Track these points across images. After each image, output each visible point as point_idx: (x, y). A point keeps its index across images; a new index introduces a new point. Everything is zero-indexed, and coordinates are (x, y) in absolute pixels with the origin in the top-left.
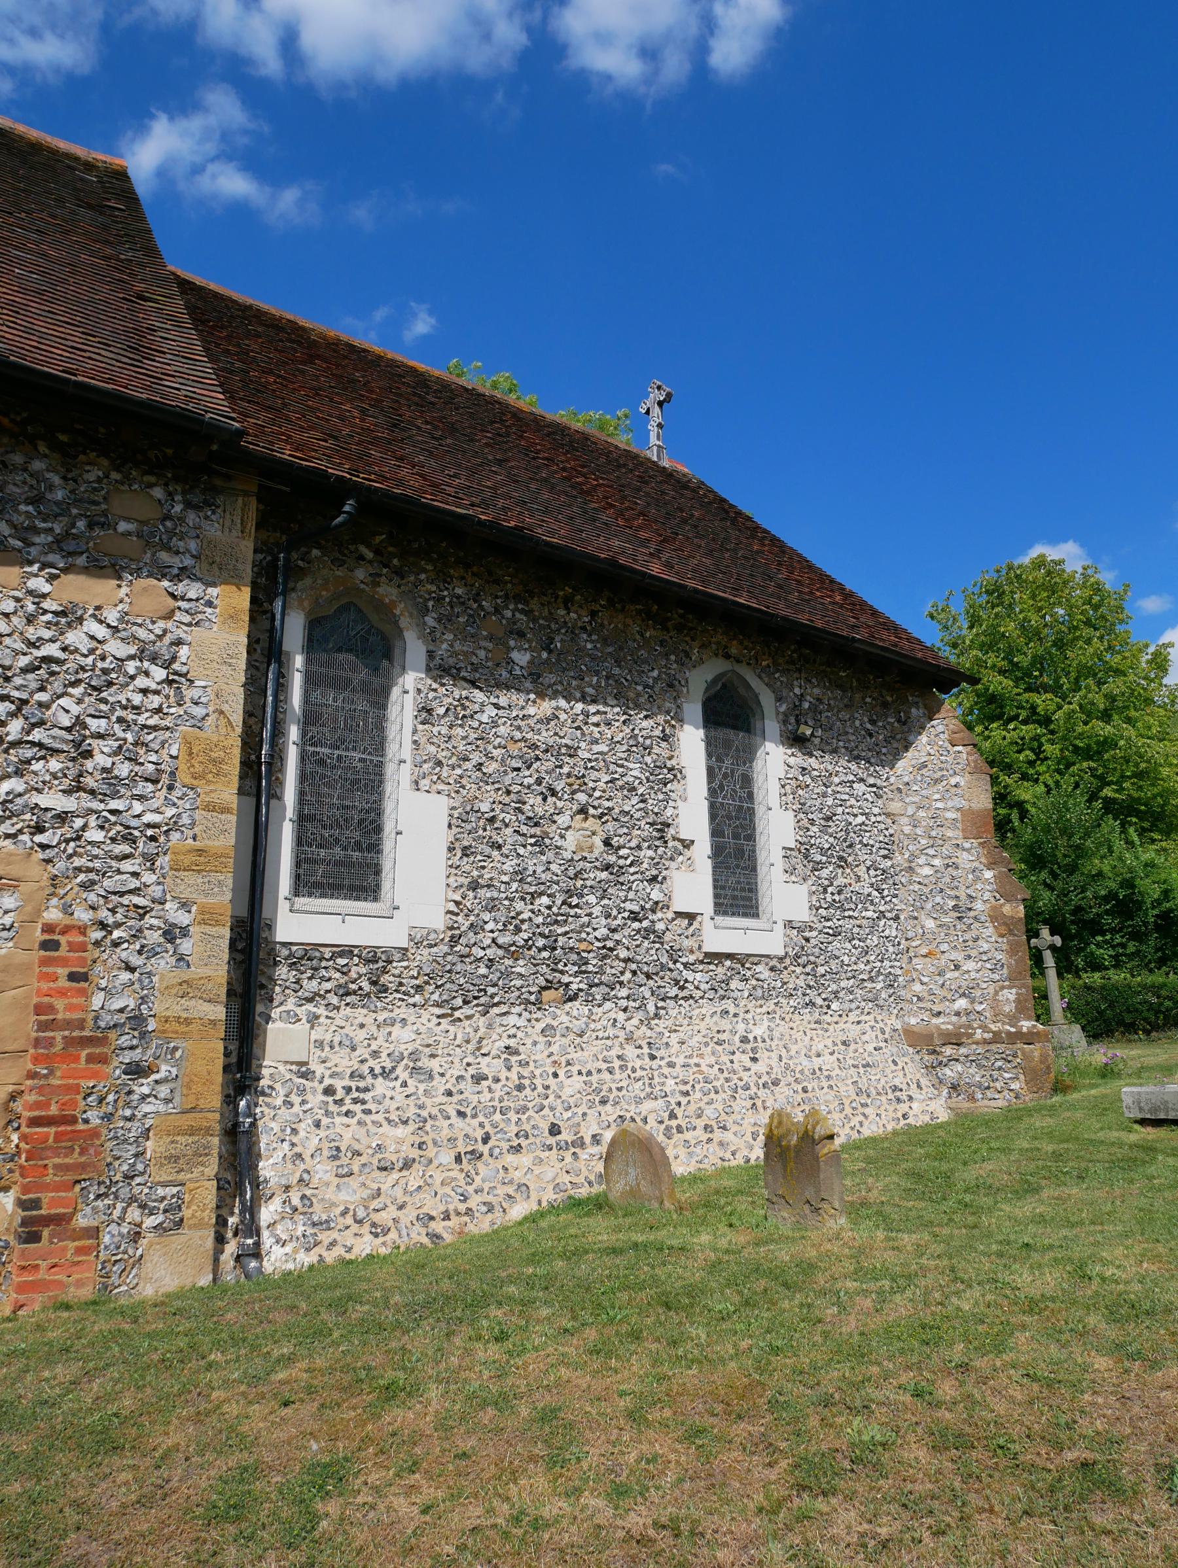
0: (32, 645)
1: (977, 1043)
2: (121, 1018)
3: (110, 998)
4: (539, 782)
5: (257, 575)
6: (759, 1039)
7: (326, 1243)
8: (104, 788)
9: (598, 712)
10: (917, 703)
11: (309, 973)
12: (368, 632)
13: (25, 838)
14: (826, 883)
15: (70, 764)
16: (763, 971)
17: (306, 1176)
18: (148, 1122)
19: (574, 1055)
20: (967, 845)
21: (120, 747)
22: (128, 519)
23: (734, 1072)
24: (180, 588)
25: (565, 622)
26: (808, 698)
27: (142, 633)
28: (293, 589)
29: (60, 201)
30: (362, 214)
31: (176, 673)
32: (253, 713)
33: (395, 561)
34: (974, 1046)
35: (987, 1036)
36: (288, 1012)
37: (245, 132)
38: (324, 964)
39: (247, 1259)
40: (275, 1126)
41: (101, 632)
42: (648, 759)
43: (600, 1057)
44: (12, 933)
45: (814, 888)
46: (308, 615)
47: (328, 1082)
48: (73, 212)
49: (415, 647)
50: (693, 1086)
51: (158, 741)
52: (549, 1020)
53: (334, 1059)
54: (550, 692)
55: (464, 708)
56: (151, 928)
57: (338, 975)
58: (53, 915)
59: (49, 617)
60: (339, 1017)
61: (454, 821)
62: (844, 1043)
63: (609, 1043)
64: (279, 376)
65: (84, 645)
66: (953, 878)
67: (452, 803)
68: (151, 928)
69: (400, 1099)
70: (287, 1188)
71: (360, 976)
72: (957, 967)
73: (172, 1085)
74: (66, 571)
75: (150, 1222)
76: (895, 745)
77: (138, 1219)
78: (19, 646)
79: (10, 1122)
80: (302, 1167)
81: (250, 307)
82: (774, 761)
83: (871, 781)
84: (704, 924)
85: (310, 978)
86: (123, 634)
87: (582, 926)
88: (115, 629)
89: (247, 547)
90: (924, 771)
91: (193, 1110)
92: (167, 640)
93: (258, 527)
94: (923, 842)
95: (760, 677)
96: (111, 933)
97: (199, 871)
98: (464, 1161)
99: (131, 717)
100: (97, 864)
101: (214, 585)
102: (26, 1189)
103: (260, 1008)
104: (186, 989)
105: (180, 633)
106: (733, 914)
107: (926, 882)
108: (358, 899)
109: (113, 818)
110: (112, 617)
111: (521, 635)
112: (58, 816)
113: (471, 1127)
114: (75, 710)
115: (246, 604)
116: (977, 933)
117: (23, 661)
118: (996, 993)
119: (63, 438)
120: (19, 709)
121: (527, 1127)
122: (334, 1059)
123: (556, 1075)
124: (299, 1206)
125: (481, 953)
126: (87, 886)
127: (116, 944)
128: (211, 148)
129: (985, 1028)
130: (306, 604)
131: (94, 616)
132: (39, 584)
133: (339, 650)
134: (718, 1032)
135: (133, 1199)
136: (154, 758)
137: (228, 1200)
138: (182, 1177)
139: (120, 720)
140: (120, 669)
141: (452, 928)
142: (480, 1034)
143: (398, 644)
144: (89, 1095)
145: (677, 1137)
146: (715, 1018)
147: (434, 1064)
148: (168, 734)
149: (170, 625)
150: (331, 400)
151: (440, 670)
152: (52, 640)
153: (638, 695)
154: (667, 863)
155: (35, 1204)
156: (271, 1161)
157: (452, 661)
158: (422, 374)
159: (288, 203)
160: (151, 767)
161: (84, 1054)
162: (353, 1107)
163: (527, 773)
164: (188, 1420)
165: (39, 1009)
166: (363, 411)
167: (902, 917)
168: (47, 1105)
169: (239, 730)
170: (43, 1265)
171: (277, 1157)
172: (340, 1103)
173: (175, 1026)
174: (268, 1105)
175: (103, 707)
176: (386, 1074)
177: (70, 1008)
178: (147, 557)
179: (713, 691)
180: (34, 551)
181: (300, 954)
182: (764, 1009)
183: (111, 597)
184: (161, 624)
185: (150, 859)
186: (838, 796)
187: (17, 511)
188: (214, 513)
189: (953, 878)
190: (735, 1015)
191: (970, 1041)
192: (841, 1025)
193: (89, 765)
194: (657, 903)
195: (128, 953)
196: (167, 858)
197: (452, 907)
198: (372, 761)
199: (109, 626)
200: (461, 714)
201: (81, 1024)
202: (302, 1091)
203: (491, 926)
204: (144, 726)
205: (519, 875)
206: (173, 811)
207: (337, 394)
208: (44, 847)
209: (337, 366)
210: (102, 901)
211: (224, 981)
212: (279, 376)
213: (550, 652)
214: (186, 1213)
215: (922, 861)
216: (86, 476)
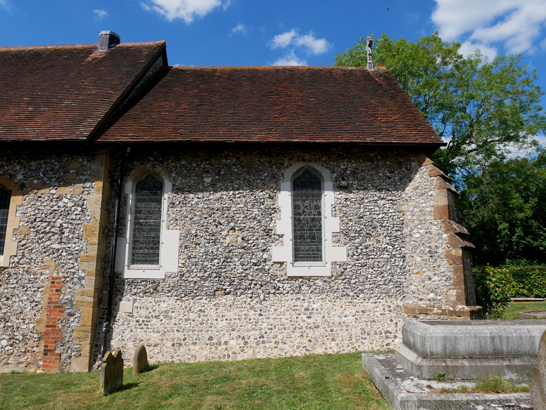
1: (435, 314)
2: (67, 301)
4: (214, 221)
6: (315, 309)
8: (67, 242)
9: (239, 193)
10: (414, 160)
14: (358, 245)
16: (319, 283)
17: (124, 346)
19: (226, 313)
20: (435, 223)
22: (73, 169)
23: (297, 322)
25: (226, 164)
26: (349, 169)
33: (160, 159)
34: (434, 316)
35: (440, 311)
40: (118, 330)
42: (262, 207)
43: (237, 314)
45: (350, 248)
49: (168, 185)
50: (275, 326)
52: (217, 301)
54: (219, 189)
55: (186, 201)
58: (55, 275)
60: (143, 300)
61: (182, 238)
62: (363, 312)
63: (242, 309)
66: (429, 238)
67: (181, 232)
69: (159, 325)
72: (430, 279)
76: (405, 180)
80: (124, 343)
82: (329, 198)
83: (390, 198)
84: (288, 265)
87: (232, 269)
90: (417, 191)
94: (417, 222)
95: (322, 165)
98: (175, 346)
101: (94, 182)
104: (83, 294)
106: (308, 260)
107: (417, 240)
108: (152, 264)
111: (208, 172)
113: (180, 335)
116: (439, 263)
118: (447, 291)
121: (200, 337)
123: (217, 320)
125: (191, 279)
129: (439, 308)
132: (53, 191)
134: (294, 306)
138: (81, 343)
140: (71, 210)
141: (180, 272)
142: (191, 305)
145: (262, 345)
146: (293, 301)
151: (177, 190)
153: (258, 184)
154: (270, 244)
157: (181, 186)
162: (144, 327)
163: (210, 218)
167: (407, 256)
169: (99, 222)
171: (117, 339)
173: (80, 303)
176: (156, 317)
177: (55, 298)
179: (296, 176)
180: (52, 183)
181: (131, 281)
182: (320, 297)
183: (67, 191)
186: (367, 207)
189: (429, 238)
190: (303, 300)
191: (431, 313)
192: (365, 304)
193: (64, 236)
194: (266, 259)
197: (181, 265)
200: (184, 203)
201: (57, 303)
203: (195, 270)
205: (206, 253)
213: (220, 175)
214: (82, 353)
215: (415, 231)
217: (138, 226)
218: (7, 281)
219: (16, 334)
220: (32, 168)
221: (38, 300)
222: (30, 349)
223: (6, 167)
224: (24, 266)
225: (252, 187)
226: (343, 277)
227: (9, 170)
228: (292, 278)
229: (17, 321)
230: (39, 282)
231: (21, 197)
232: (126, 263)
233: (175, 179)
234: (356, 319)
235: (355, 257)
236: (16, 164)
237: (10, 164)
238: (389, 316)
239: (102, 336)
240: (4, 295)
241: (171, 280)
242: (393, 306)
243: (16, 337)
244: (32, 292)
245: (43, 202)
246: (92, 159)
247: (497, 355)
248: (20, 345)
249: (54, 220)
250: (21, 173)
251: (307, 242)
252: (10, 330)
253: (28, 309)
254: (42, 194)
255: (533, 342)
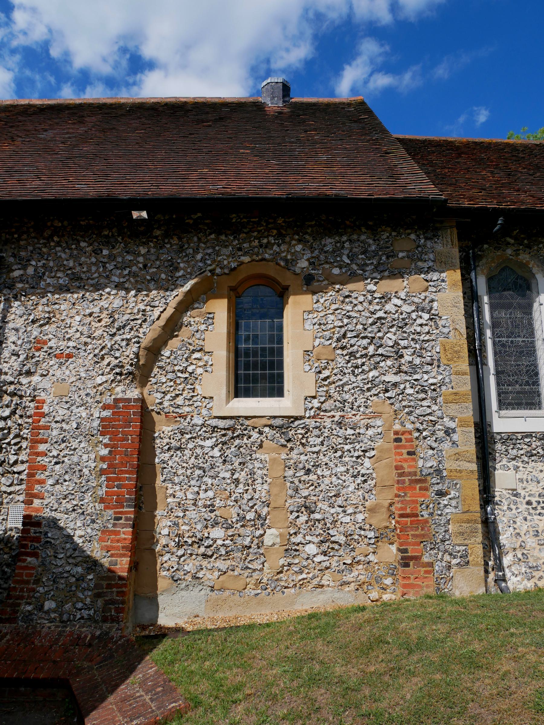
0: (372, 313)
2: (431, 471)
3: (426, 462)
5: (461, 262)
7: (537, 577)
11: (512, 446)
12: (517, 279)
13: (381, 395)
15: (395, 362)
17: (523, 544)
18: (449, 517)
21: (415, 351)
22: (402, 251)
24: (429, 277)
27: (416, 300)
28: (478, 266)
29: (344, 124)
30: (441, 72)
31: (433, 315)
32: (470, 326)
33: (526, 241)
36: (504, 465)
37: (380, 55)
38: (518, 441)
39: (500, 582)
41: (399, 302)
44: (382, 436)
46: (486, 277)
47: (527, 498)
48: (350, 127)
51: (430, 346)
53: (529, 488)
56: (439, 430)
57: (526, 447)
59: (377, 300)
64: (449, 168)
65: (393, 309)
68: (439, 430)
70: (515, 549)
71: (537, 447)
73: (457, 500)
74: (381, 279)
75: (454, 562)
77: (449, 560)
78: (368, 314)
79: (391, 515)
80: (521, 539)
81: (426, 140)
85: (512, 449)
86: (408, 302)
88: (405, 300)
89: (455, 252)
91: (467, 512)
92: (427, 301)
93: (459, 240)
96: (422, 433)
97: (456, 403)
99: (417, 337)
100: (412, 404)
101: (443, 272)
102: (401, 544)
103: (491, 464)
104: (458, 456)
105: (432, 296)
108: (531, 409)
109: (416, 383)
110: (402, 295)
112: (393, 384)
114: (394, 338)
115: (459, 277)
117: (370, 321)
119: (371, 223)
120: (372, 341)
122: (529, 488)
124: (522, 558)
126: (409, 413)
127: (425, 438)
128: (368, 69)
130: (485, 271)
131: (395, 296)
132: (372, 287)
133: (504, 290)
135: (446, 551)
136: (429, 354)
137: (488, 554)
139: (413, 339)
143: (533, 281)
144: (422, 504)
148: (434, 342)
149: (427, 294)
150: (476, 172)
152: (380, 310)
155: (405, 551)
156: (505, 536)
158: (513, 145)
159: (407, 80)
160: (429, 358)
161: (418, 486)
164: (510, 659)
165: (397, 468)
166: (492, 172)
168: (405, 509)
169: (465, 336)
170: (412, 577)
171: (508, 534)
172: (535, 509)
173: (455, 474)
174: (500, 509)
175: (405, 335)
177: (410, 467)
178: (413, 266)
180: (367, 274)
181: (506, 437)
184: (424, 294)
185: (434, 399)
187: (358, 259)
188: (438, 239)
193: (403, 361)
195: (430, 442)
196: (442, 398)
198: (528, 341)
199: (402, 299)
201: (415, 474)
202: (516, 503)
204: (423, 341)
206: (441, 377)
207: (477, 168)
208: (389, 398)
209: (472, 154)
210: (416, 420)
211: (474, 452)
212: (449, 168)
214: (470, 558)
216: (382, 237)
218: (304, 441)
219: (331, 532)
220: (326, 249)
221: (368, 472)
222: (363, 558)
223: (275, 248)
224: (332, 413)
227: (283, 252)
229: (332, 511)
230: (366, 440)
231: (310, 296)
236: (294, 242)
237: (284, 242)
240: (301, 466)
243: (333, 539)
244: (354, 459)
245: (356, 305)
246: (435, 236)
248: (341, 552)
249: (380, 334)
250: (305, 257)
252: (320, 526)
253: (351, 489)
254: (351, 292)
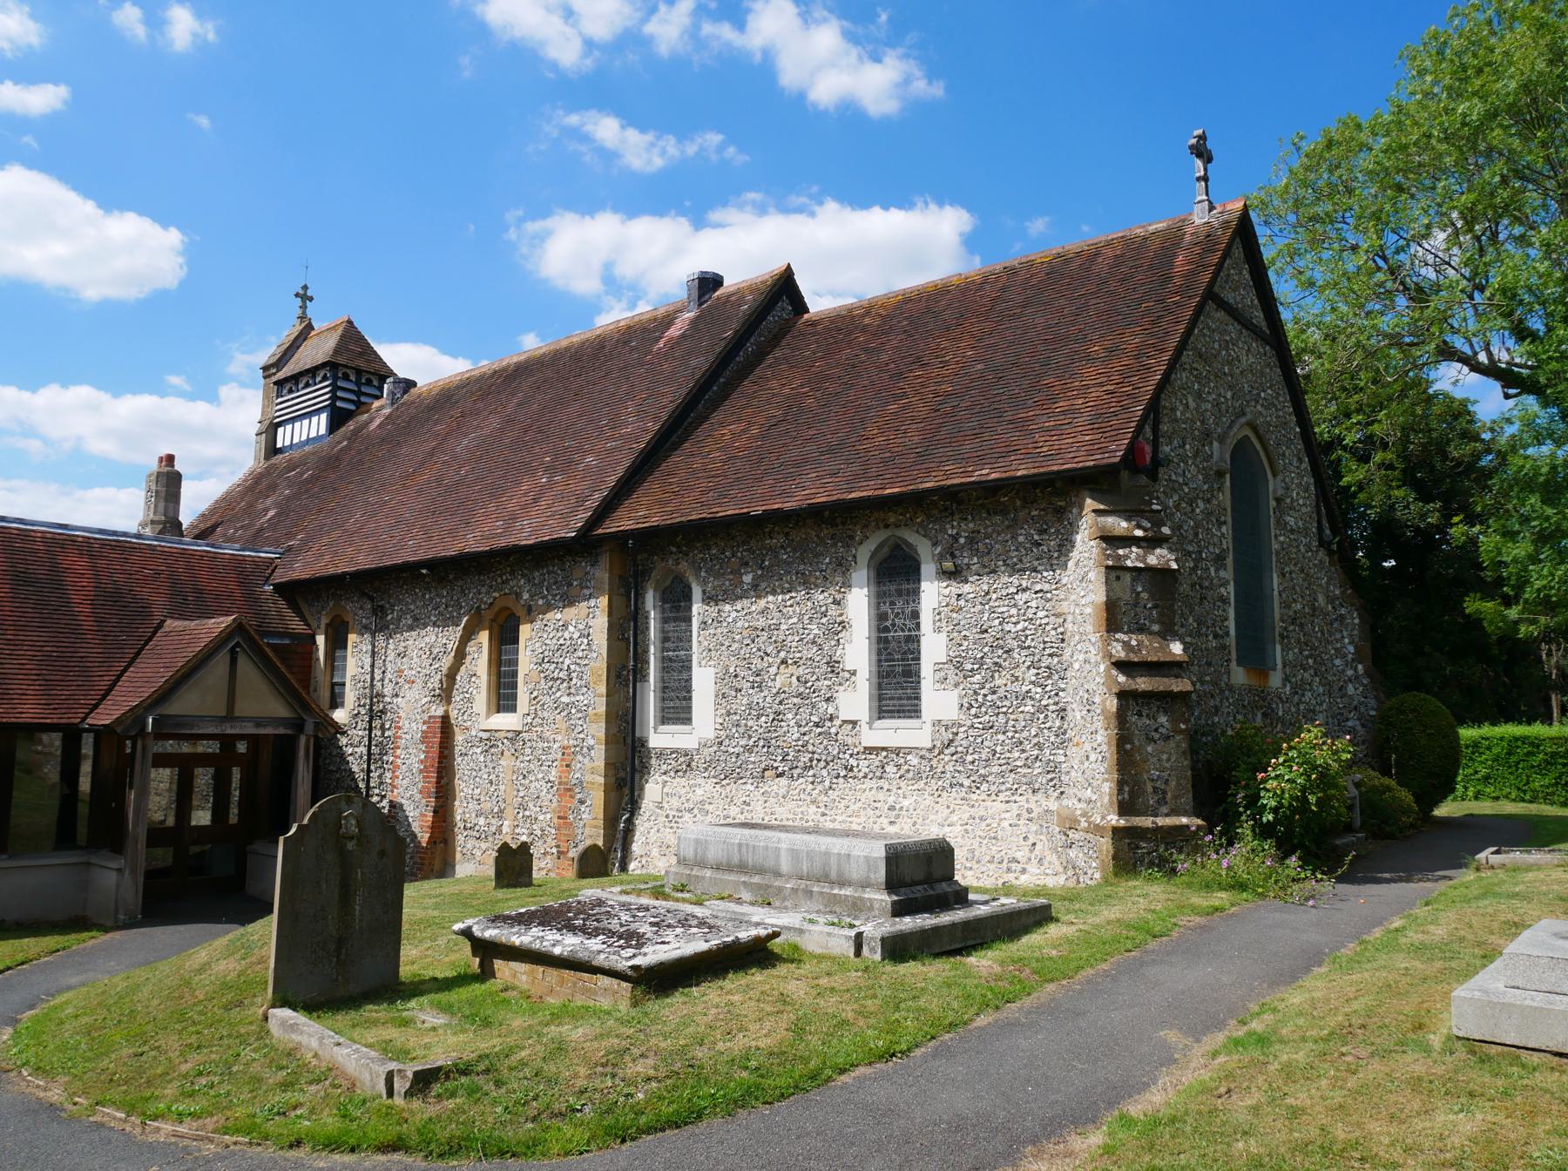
16: (914, 760)
42: (824, 620)
62: (981, 819)
82: (932, 593)
83: (1038, 587)
111: (747, 564)
132: (559, 616)
147: (710, 808)
151: (709, 599)
192: (988, 803)
217: (667, 665)
225: (807, 584)
226: (952, 749)
228: (870, 750)
232: (652, 724)
233: (705, 582)
234: (967, 831)
235: (973, 711)
238: (1024, 829)
239: (620, 836)
241: (706, 751)
242: (1037, 810)
247: (742, 868)
251: (897, 685)
255: (778, 856)
